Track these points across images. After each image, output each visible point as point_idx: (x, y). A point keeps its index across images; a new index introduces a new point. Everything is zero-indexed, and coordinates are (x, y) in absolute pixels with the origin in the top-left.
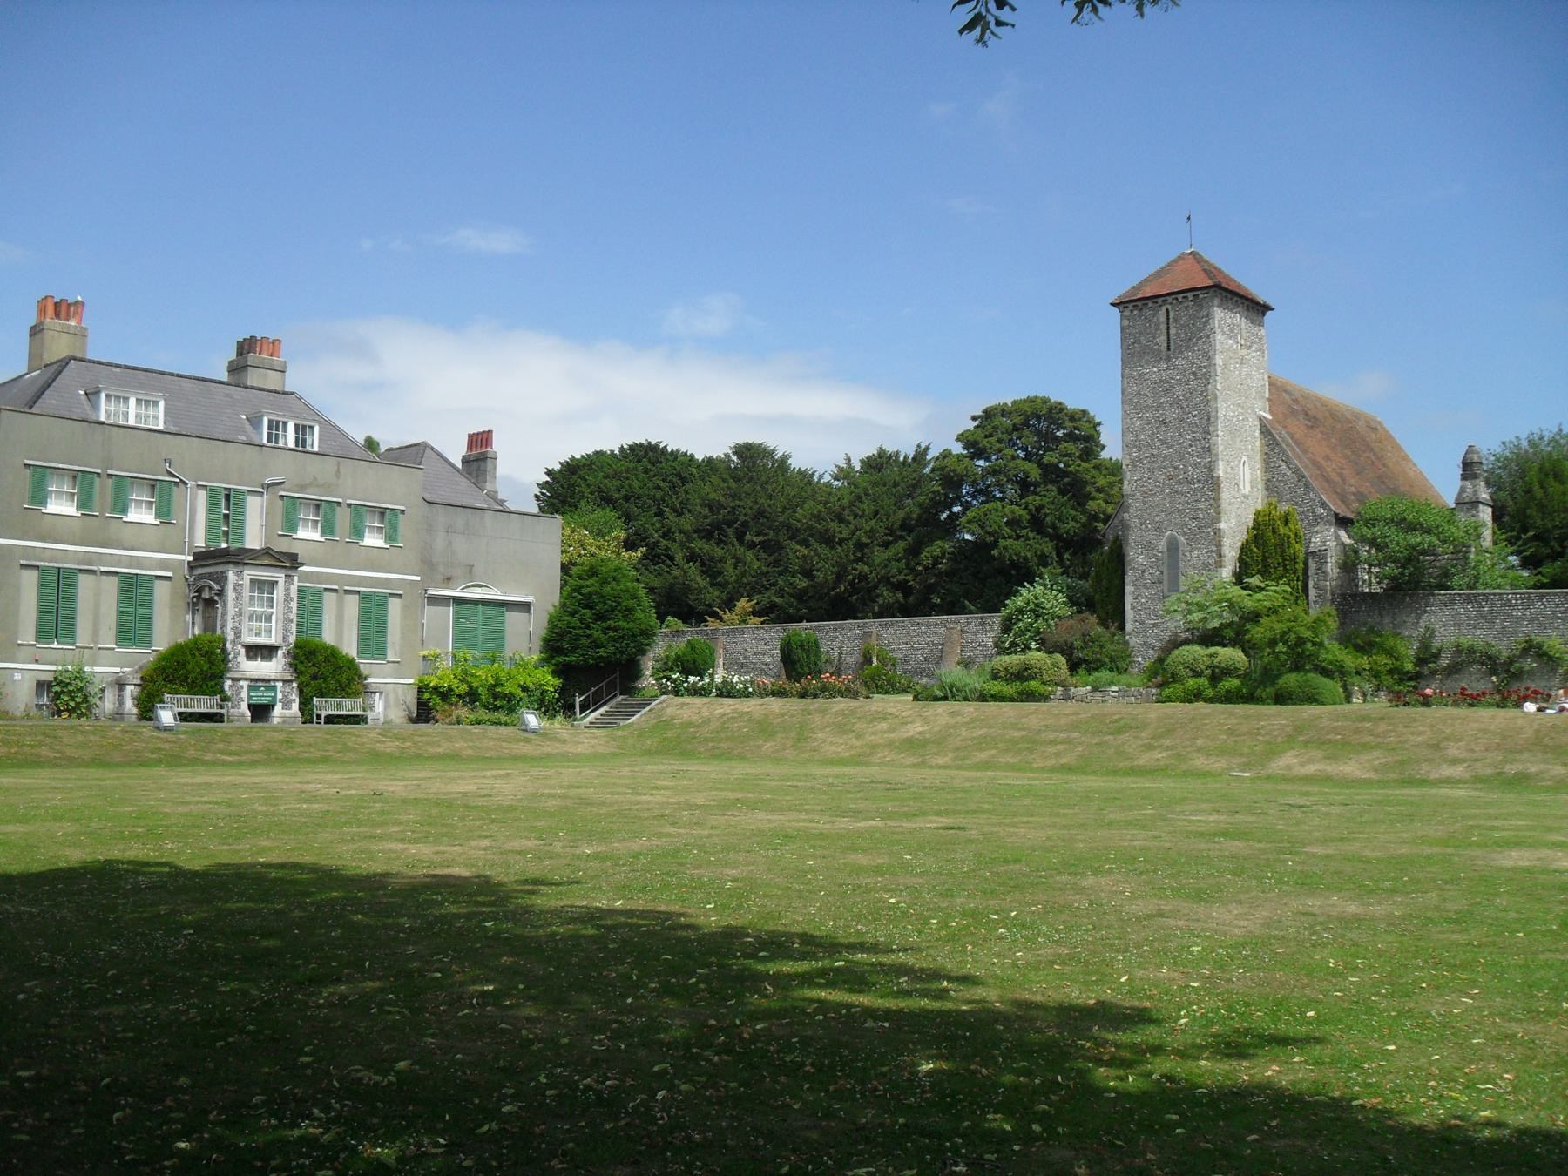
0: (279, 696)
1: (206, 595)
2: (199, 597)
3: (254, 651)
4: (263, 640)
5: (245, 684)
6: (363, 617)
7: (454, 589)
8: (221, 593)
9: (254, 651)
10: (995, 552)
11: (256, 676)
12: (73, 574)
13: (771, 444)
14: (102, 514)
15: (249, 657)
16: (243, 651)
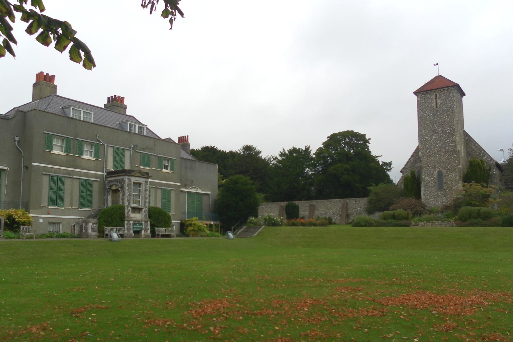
0: (144, 227)
1: (114, 188)
2: (110, 189)
3: (135, 210)
4: (137, 205)
5: (132, 222)
6: (163, 198)
7: (187, 188)
8: (122, 187)
9: (135, 210)
10: (341, 179)
11: (135, 219)
12: (63, 178)
16: (131, 209)
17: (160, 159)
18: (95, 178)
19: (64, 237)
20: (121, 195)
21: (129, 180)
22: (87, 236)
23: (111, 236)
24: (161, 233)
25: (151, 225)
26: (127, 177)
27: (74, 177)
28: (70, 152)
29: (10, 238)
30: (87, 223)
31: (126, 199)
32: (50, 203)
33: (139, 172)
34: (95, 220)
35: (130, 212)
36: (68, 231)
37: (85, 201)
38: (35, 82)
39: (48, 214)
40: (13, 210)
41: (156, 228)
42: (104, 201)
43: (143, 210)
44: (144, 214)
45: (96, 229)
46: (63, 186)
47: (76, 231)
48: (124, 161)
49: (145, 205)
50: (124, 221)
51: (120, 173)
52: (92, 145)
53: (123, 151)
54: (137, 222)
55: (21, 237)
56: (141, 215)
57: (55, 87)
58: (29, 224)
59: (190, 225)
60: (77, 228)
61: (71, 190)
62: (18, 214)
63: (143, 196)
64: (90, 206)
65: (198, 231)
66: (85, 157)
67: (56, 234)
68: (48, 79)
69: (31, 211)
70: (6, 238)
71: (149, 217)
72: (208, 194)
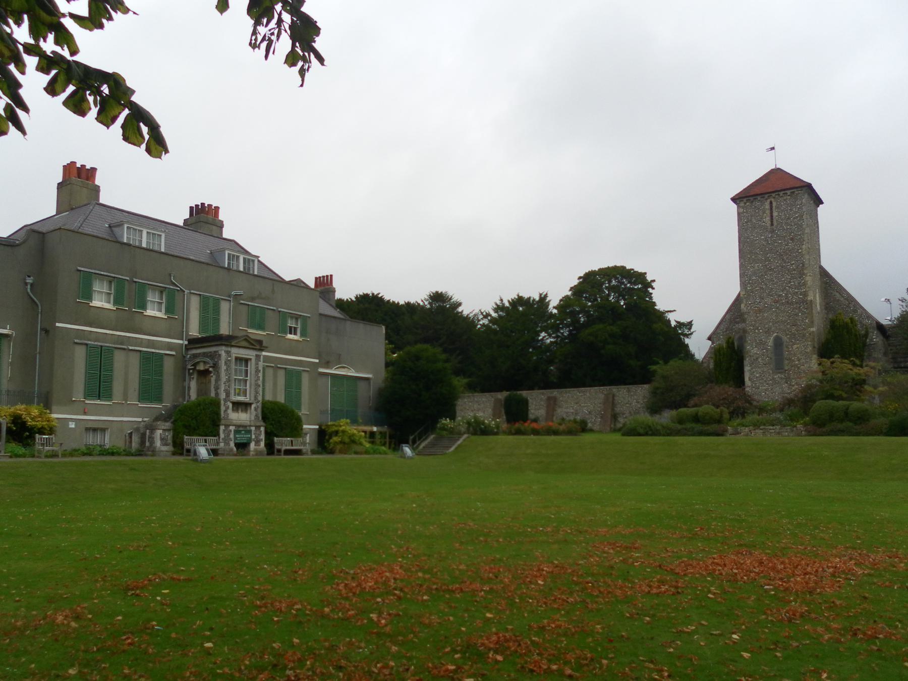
0: (253, 437)
1: (201, 367)
4: (241, 398)
5: (232, 428)
6: (288, 386)
8: (215, 366)
9: (239, 406)
11: (239, 423)
12: (110, 351)
13: (450, 294)
16: (231, 405)
17: (283, 316)
19: (113, 454)
20: (213, 379)
21: (228, 353)
22: (154, 452)
23: (195, 453)
24: (284, 448)
25: (266, 433)
26: (224, 348)
28: (123, 305)
29: (17, 456)
30: (152, 429)
31: (223, 388)
33: (246, 340)
34: (168, 425)
36: (120, 444)
37: (150, 390)
39: (85, 413)
42: (183, 391)
43: (253, 406)
44: (254, 413)
46: (112, 364)
47: (133, 444)
49: (256, 398)
50: (218, 426)
52: (161, 292)
53: (217, 302)
54: (241, 428)
55: (36, 454)
57: (97, 189)
58: (51, 431)
60: (136, 439)
61: (126, 372)
62: (32, 413)
63: (253, 382)
64: (159, 399)
65: (350, 444)
66: (150, 312)
68: (83, 175)
69: (54, 408)
70: (11, 457)
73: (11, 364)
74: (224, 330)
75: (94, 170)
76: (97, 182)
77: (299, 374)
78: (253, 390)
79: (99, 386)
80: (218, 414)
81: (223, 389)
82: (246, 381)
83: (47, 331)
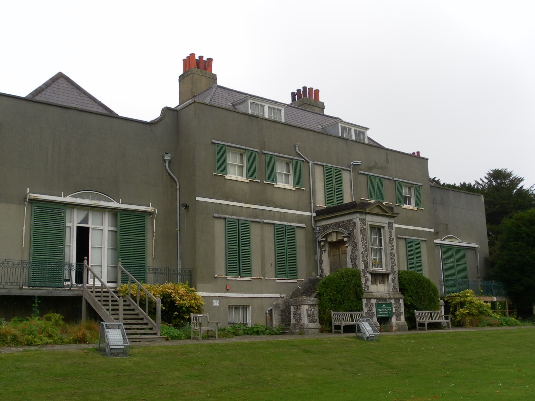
0: (394, 310)
1: (334, 238)
4: (378, 269)
5: (373, 301)
6: (409, 257)
8: (350, 235)
9: (380, 277)
11: (378, 295)
14: (262, 181)
15: (374, 282)
17: (398, 185)
18: (298, 223)
19: (258, 333)
20: (349, 250)
21: (363, 221)
22: (302, 331)
23: (359, 331)
24: (344, 323)
25: (406, 305)
26: (358, 215)
27: (265, 221)
28: (254, 177)
29: (173, 338)
30: (298, 306)
31: (361, 258)
32: (230, 270)
33: (378, 206)
34: (313, 300)
35: (369, 283)
36: (262, 322)
37: (285, 266)
38: (181, 73)
39: (227, 290)
40: (170, 285)
41: (416, 312)
42: (317, 265)
43: (390, 277)
44: (392, 284)
45: (316, 318)
46: (249, 239)
47: (274, 322)
48: (341, 190)
49: (392, 268)
50: (361, 299)
51: (328, 214)
52: (288, 164)
53: (339, 173)
54: (382, 302)
55: (192, 336)
56: (386, 287)
57: (214, 78)
58: (199, 310)
59: (462, 305)
60: (276, 316)
61: (262, 245)
62: (179, 291)
63: (388, 252)
64: (294, 273)
65: (477, 317)
66: (280, 184)
67: (242, 328)
68: (201, 65)
69: (199, 285)
70: (167, 339)
71: (400, 290)
72: (474, 249)
73: (155, 242)
74: (347, 199)
75: (210, 60)
76: (214, 71)
77: (418, 244)
78: (389, 260)
79: (239, 263)
80: (360, 286)
81: (361, 259)
82: (380, 250)
83: (186, 207)
